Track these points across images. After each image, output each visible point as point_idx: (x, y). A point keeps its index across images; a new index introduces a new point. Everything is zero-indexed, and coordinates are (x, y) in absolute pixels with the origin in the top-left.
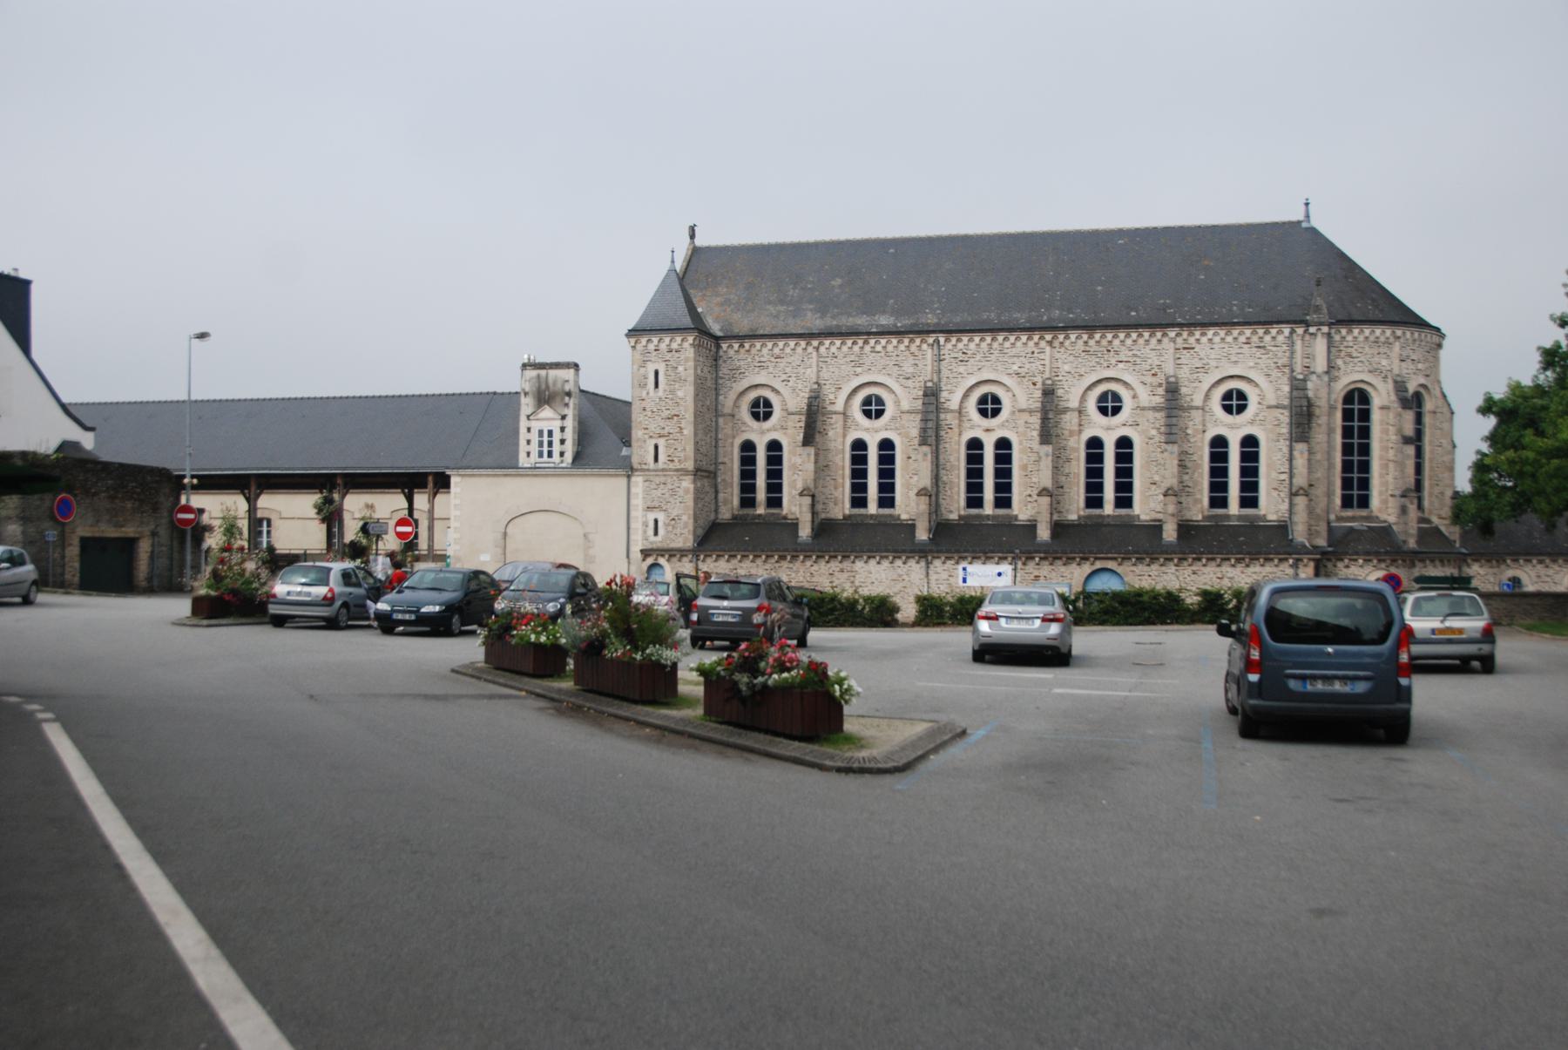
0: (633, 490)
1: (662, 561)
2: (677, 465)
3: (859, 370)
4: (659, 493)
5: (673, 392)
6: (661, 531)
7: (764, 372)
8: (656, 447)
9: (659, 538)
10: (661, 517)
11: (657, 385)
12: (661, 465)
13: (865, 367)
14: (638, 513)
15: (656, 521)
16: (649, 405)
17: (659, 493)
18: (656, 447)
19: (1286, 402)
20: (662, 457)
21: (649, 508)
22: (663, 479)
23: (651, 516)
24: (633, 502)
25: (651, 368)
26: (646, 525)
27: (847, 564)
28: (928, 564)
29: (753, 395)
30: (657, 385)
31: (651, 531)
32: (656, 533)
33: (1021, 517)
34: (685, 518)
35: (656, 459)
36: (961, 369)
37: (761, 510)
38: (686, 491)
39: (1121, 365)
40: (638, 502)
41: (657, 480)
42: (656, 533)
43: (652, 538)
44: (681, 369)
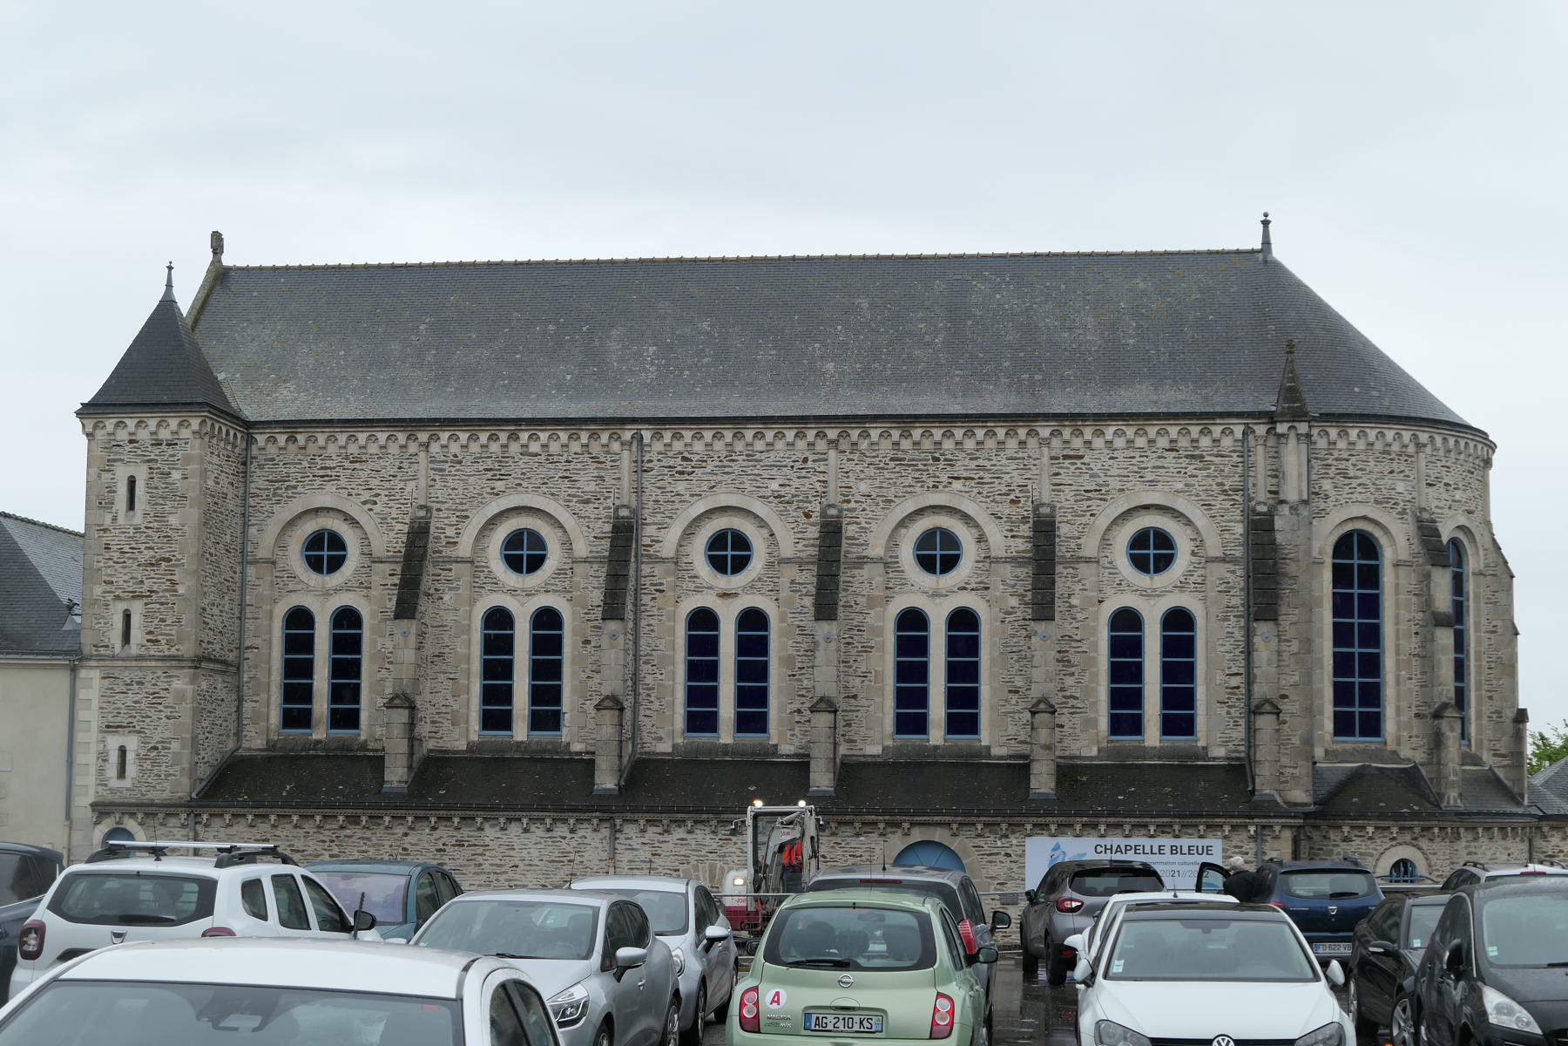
0: (82, 694)
3: (500, 485)
4: (129, 699)
6: (132, 770)
8: (127, 617)
9: (127, 783)
12: (134, 649)
13: (512, 481)
14: (89, 736)
15: (123, 751)
16: (115, 538)
17: (129, 699)
18: (127, 617)
20: (137, 635)
21: (110, 728)
23: (114, 742)
24: (81, 715)
25: (122, 473)
26: (103, 757)
27: (466, 832)
29: (310, 527)
31: (112, 771)
32: (122, 773)
34: (175, 746)
35: (126, 637)
36: (681, 487)
37: (320, 732)
39: (957, 485)
40: (90, 716)
41: (127, 676)
42: (122, 773)
43: (114, 783)
44: (176, 475)
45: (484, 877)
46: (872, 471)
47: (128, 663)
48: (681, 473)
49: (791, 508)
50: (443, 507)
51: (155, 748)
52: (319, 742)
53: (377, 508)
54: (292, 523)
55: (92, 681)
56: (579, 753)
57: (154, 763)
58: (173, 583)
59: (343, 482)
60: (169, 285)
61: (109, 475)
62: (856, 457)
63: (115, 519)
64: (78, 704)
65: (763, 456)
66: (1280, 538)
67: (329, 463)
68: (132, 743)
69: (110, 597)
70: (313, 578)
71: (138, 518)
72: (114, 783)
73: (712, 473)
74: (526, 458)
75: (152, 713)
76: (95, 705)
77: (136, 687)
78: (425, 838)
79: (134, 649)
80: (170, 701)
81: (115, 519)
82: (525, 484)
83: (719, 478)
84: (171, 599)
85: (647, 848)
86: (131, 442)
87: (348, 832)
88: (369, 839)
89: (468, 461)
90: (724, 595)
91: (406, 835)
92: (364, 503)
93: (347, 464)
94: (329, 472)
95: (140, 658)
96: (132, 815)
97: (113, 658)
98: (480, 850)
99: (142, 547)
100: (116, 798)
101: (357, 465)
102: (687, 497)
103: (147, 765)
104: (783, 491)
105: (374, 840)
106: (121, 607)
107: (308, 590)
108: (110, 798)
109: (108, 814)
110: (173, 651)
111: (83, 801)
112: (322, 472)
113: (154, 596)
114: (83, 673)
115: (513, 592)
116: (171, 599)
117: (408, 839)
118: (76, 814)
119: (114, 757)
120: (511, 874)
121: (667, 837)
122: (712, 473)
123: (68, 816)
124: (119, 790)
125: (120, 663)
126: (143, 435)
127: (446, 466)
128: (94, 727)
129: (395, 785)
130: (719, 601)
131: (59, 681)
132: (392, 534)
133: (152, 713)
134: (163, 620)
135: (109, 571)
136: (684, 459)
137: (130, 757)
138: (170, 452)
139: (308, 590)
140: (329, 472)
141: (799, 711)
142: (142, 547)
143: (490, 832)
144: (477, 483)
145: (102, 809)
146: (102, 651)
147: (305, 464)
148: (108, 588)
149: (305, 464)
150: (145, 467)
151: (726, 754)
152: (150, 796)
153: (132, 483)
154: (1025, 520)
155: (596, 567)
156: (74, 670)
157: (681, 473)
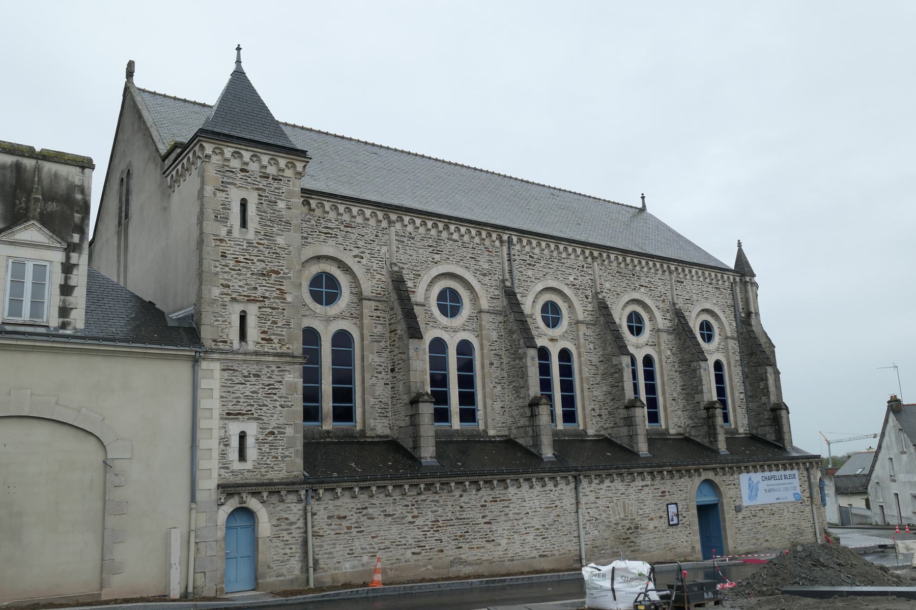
0: (204, 384)
1: (253, 503)
2: (277, 347)
3: (437, 257)
4: (248, 389)
5: (268, 236)
6: (252, 453)
7: (331, 242)
8: (243, 318)
9: (249, 465)
10: (252, 429)
11: (244, 224)
12: (251, 346)
13: (444, 256)
14: (211, 423)
15: (242, 437)
16: (231, 249)
17: (248, 389)
18: (243, 318)
19: (735, 335)
20: (253, 333)
21: (231, 415)
22: (254, 368)
23: (235, 428)
24: (204, 403)
25: (235, 195)
26: (225, 442)
27: (498, 492)
28: (577, 481)
29: (315, 269)
30: (244, 224)
31: (234, 454)
32: (242, 457)
33: (591, 432)
34: (289, 431)
35: (243, 336)
36: (530, 273)
37: (328, 425)
38: (292, 387)
39: (642, 289)
40: (212, 404)
41: (245, 369)
42: (242, 457)
43: (237, 466)
44: (281, 205)
45: (510, 523)
46: (610, 277)
47: (248, 357)
48: (530, 265)
49: (580, 292)
50: (406, 266)
51: (272, 433)
52: (328, 432)
53: (364, 261)
54: (319, 258)
55: (213, 374)
56: (494, 437)
57: (272, 446)
58: (282, 292)
59: (340, 240)
60: (238, 62)
61: (224, 195)
62: (603, 268)
63: (229, 232)
64: (200, 394)
65: (566, 261)
66: (754, 328)
67: (330, 225)
68: (252, 429)
69: (227, 299)
70: (318, 308)
71: (251, 235)
72: (237, 466)
73: (543, 267)
74: (451, 243)
75: (268, 402)
76: (217, 394)
77: (253, 379)
78: (473, 497)
79: (251, 346)
80: (283, 392)
81: (229, 232)
82: (451, 258)
83: (547, 270)
84: (281, 306)
85: (593, 494)
86: (242, 170)
87: (423, 497)
88: (437, 501)
89: (418, 238)
90: (552, 340)
91: (461, 496)
92: (355, 256)
93: (342, 227)
94: (330, 231)
95: (256, 353)
96: (254, 494)
97: (233, 352)
98: (506, 503)
99: (255, 259)
100: (238, 480)
101: (349, 229)
102: (533, 279)
103: (266, 449)
104: (576, 282)
105: (441, 502)
106: (237, 308)
107: (315, 315)
108: (232, 479)
109: (230, 495)
110: (284, 350)
111: (208, 484)
112: (325, 230)
113: (267, 302)
114: (204, 365)
115: (445, 328)
116: (281, 306)
117: (463, 499)
118: (200, 496)
119: (235, 442)
120: (525, 519)
121: (602, 486)
122: (543, 267)
123: (193, 499)
124: (241, 472)
125: (240, 357)
126: (254, 167)
127: (405, 239)
128: (216, 414)
129: (429, 460)
130: (550, 343)
131: (180, 371)
132: (374, 281)
133: (268, 402)
134: (275, 323)
135: (225, 276)
136: (530, 257)
137: (250, 441)
138: (276, 185)
139: (315, 315)
140: (330, 231)
141: (593, 410)
142: (255, 259)
143: (512, 490)
144: (424, 254)
145: (228, 490)
146: (221, 346)
147: (313, 222)
148: (226, 290)
149: (313, 222)
150: (256, 193)
151: (565, 436)
152: (269, 476)
153: (244, 204)
154: (668, 311)
155: (493, 316)
156: (196, 361)
157: (530, 265)
